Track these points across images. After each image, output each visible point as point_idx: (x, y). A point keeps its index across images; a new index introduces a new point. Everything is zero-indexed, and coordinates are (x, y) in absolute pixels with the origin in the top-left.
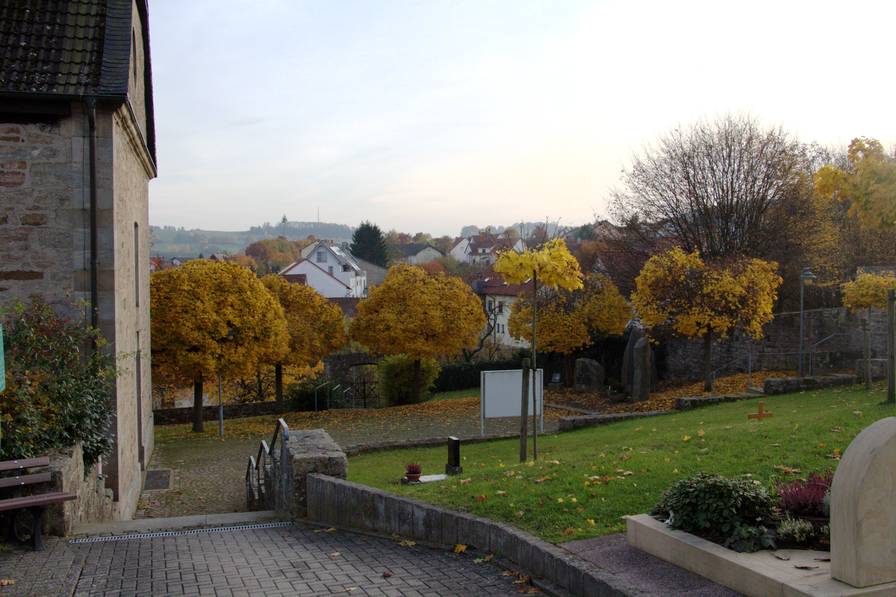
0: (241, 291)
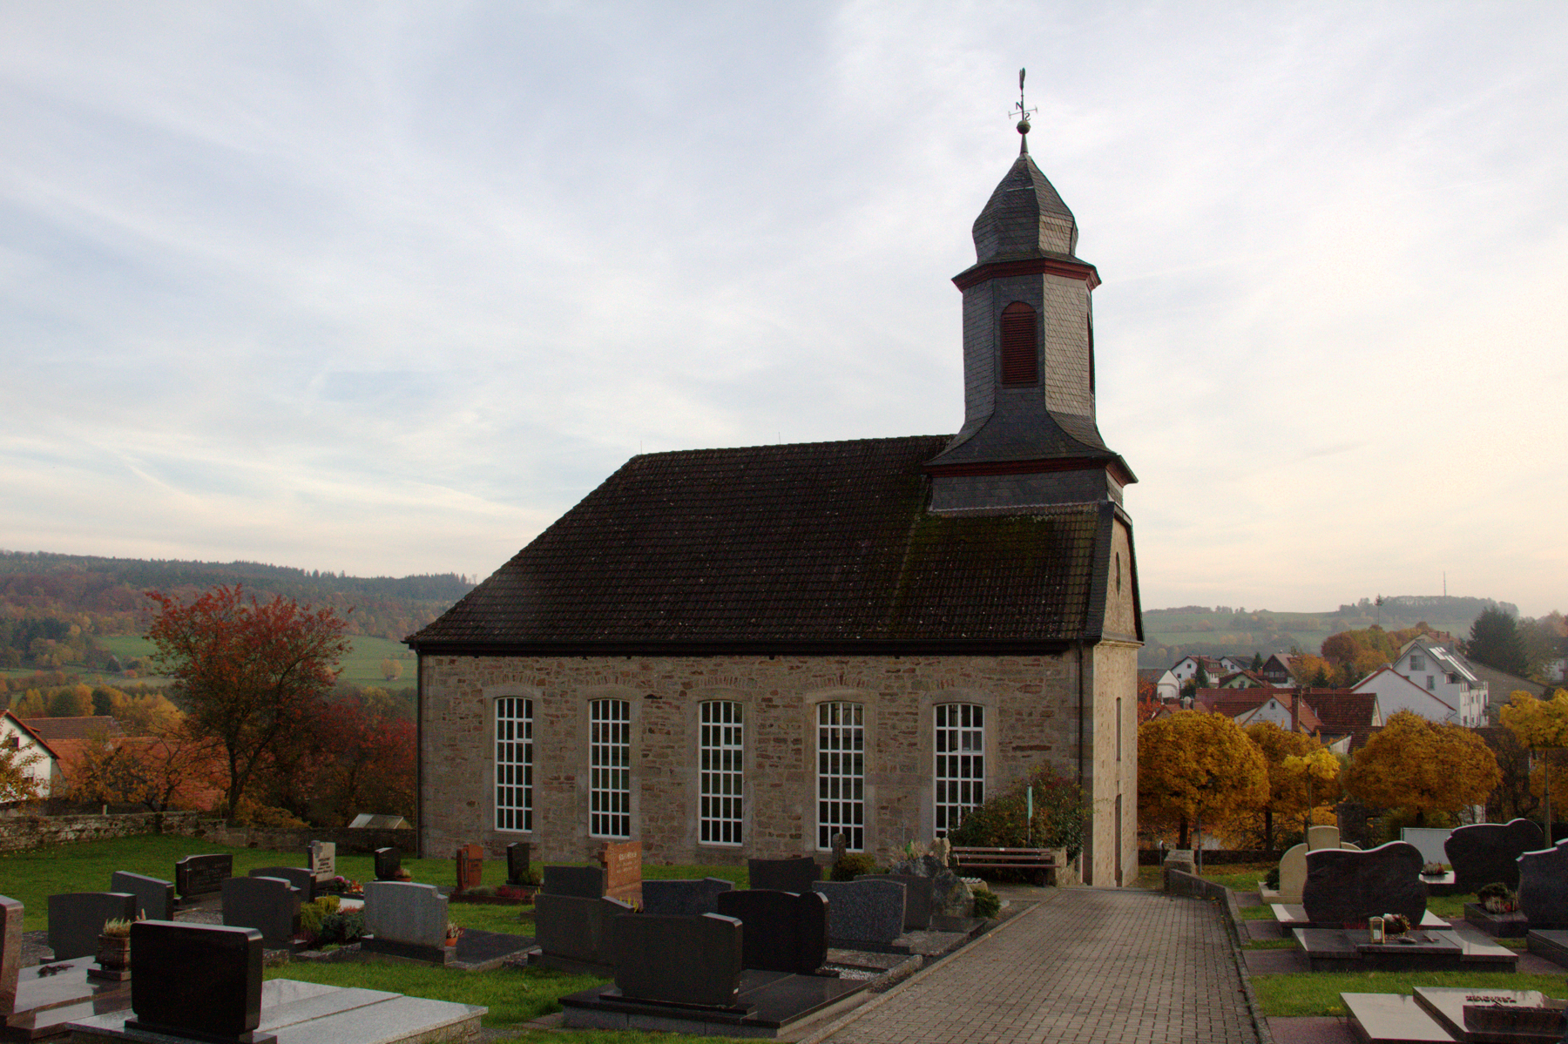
0: (1220, 742)
